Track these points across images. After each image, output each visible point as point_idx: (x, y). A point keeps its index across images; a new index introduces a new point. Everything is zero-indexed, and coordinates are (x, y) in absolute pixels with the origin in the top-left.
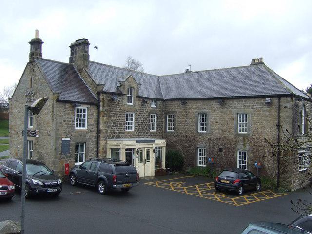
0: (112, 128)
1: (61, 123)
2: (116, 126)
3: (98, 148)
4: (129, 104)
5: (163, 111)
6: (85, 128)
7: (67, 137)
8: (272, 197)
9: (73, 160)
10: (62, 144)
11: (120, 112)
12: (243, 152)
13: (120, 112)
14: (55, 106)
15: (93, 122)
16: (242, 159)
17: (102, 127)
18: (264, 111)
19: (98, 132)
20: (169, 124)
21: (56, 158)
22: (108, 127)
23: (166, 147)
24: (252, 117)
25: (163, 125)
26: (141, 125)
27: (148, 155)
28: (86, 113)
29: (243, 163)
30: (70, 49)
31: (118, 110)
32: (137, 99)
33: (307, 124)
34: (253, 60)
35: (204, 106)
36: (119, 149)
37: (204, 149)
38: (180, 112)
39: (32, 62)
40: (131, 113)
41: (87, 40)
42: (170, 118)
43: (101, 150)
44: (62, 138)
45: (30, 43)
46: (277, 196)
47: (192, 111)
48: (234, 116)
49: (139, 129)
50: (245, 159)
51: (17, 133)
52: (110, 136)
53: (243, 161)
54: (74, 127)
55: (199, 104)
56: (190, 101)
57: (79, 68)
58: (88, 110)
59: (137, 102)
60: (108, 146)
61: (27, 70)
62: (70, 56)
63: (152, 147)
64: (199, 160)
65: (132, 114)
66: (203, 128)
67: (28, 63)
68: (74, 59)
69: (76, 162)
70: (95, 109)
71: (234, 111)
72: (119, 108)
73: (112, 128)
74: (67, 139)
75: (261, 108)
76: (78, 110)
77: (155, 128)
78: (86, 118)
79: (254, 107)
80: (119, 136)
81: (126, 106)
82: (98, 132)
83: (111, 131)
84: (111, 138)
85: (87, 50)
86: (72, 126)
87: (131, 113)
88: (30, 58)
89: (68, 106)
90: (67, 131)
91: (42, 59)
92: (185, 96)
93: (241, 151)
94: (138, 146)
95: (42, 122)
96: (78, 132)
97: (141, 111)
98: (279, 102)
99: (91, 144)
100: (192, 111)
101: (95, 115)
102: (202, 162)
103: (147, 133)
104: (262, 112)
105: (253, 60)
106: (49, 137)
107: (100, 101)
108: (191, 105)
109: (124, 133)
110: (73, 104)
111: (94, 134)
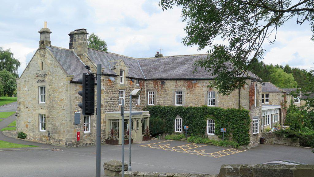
0: (109, 103)
1: (74, 100)
2: (112, 101)
4: (121, 83)
7: (78, 111)
8: (221, 152)
9: (82, 129)
10: (75, 117)
11: (114, 90)
13: (114, 90)
14: (68, 87)
16: (179, 124)
20: (150, 99)
22: (107, 102)
25: (145, 100)
27: (133, 125)
29: (211, 129)
30: (69, 37)
31: (114, 89)
32: (126, 79)
33: (258, 99)
39: (43, 49)
40: (122, 91)
41: (86, 30)
42: (151, 95)
44: (75, 111)
46: (240, 152)
49: (128, 103)
50: (180, 124)
52: (108, 109)
56: (168, 81)
57: (79, 53)
59: (127, 82)
62: (69, 43)
65: (123, 92)
66: (179, 102)
67: (38, 49)
68: (73, 46)
69: (84, 130)
73: (109, 103)
74: (78, 113)
80: (115, 109)
87: (122, 91)
88: (40, 45)
91: (50, 46)
92: (164, 76)
95: (56, 99)
102: (179, 129)
106: (64, 111)
109: (117, 107)
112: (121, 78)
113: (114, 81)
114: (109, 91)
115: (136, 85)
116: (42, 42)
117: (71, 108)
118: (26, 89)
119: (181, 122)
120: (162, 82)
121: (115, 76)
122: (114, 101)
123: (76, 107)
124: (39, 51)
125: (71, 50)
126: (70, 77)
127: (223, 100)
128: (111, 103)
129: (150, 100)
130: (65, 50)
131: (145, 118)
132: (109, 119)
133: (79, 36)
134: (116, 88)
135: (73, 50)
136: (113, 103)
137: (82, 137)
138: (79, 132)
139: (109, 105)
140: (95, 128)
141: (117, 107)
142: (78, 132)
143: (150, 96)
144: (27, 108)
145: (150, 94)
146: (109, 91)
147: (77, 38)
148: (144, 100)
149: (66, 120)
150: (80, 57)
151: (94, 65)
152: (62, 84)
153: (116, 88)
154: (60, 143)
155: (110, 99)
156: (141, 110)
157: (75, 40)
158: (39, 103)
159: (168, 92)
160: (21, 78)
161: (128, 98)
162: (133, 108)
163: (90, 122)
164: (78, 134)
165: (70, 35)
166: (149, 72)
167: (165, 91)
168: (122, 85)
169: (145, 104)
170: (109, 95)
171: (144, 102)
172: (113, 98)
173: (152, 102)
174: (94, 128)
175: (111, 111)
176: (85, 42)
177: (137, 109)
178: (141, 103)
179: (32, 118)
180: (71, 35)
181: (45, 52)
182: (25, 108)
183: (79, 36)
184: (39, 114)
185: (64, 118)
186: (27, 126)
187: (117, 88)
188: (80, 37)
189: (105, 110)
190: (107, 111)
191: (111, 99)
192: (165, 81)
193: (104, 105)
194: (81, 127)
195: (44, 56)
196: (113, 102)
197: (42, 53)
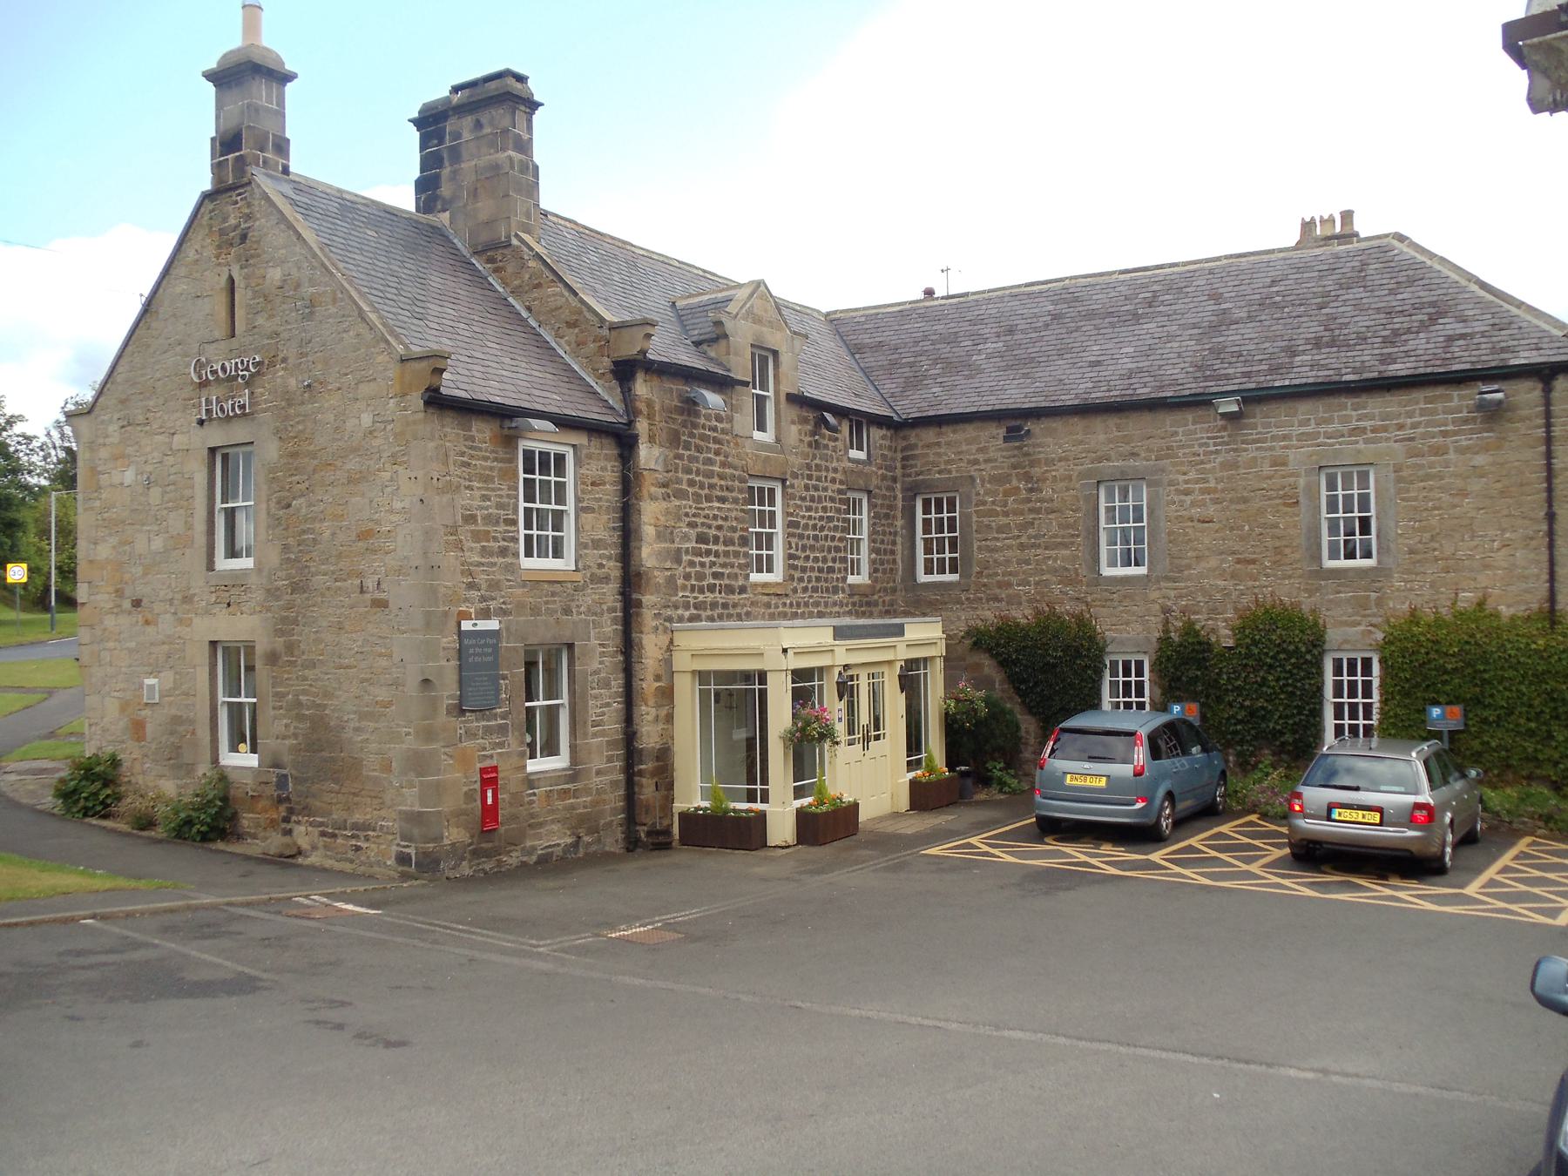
0: (692, 564)
2: (708, 552)
3: (628, 671)
4: (757, 435)
5: (894, 480)
6: (566, 564)
7: (485, 614)
11: (721, 477)
12: (1126, 665)
13: (721, 477)
15: (603, 527)
17: (648, 554)
18: (1462, 451)
19: (631, 581)
20: (928, 543)
21: (429, 734)
23: (946, 659)
24: (1399, 480)
25: (899, 547)
26: (812, 548)
28: (569, 479)
30: (414, 135)
32: (791, 413)
34: (1307, 226)
35: (1127, 440)
36: (762, 676)
37: (1359, 656)
38: (995, 480)
40: (767, 485)
41: (521, 79)
43: (648, 685)
44: (468, 617)
45: (210, 76)
47: (1060, 469)
48: (1302, 482)
51: (137, 603)
52: (687, 606)
53: (1353, 707)
54: (516, 555)
55: (1102, 432)
57: (484, 237)
58: (578, 463)
59: (794, 429)
60: (682, 662)
61: (198, 237)
62: (417, 174)
63: (890, 663)
64: (1329, 722)
65: (772, 491)
67: (206, 197)
68: (445, 190)
70: (607, 458)
71: (1297, 456)
72: (717, 453)
75: (1445, 434)
76: (529, 455)
77: (865, 567)
78: (570, 507)
79: (1408, 432)
80: (725, 606)
81: (748, 443)
82: (631, 581)
83: (687, 577)
84: (692, 619)
85: (526, 137)
86: (503, 552)
87: (767, 485)
88: (217, 168)
89: (483, 431)
90: (482, 579)
92: (1015, 395)
93: (1345, 657)
94: (843, 654)
96: (536, 583)
97: (810, 477)
98: (1548, 403)
99: (599, 658)
100: (1060, 469)
101: (609, 492)
103: (835, 590)
104: (1452, 456)
105: (1307, 226)
107: (631, 411)
108: (1052, 441)
109: (743, 590)
110: (504, 416)
111: (610, 593)
112: (761, 401)
113: (719, 419)
114: (691, 483)
115: (847, 453)
116: (227, 144)
117: (432, 592)
118: (129, 476)
119: (1146, 678)
120: (1009, 430)
121: (723, 383)
122: (721, 548)
123: (471, 586)
124: (209, 206)
125: (430, 218)
126: (424, 364)
127: (1434, 522)
128: (702, 565)
129: (928, 550)
130: (391, 213)
131: (912, 664)
132: (693, 672)
133: (484, 120)
134: (731, 466)
135: (445, 217)
136: (713, 564)
137: (516, 798)
138: (495, 769)
139: (687, 577)
140: (603, 734)
141: (743, 590)
142: (488, 763)
143: (927, 523)
144: (137, 603)
145: (926, 511)
146: (691, 483)
147: (467, 135)
148: (893, 552)
149: (396, 684)
150: (491, 260)
151: (582, 301)
152: (367, 419)
153: (731, 466)
154: (358, 848)
155: (693, 533)
156: (876, 610)
157: (455, 154)
158: (210, 566)
159: (1047, 492)
160: (97, 409)
161: (801, 537)
162: (835, 604)
163: (564, 700)
164: (489, 778)
165: (419, 123)
166: (914, 382)
167: (1031, 490)
168: (763, 446)
169: (898, 579)
170: (688, 505)
171: (894, 561)
172: (713, 532)
173: (941, 561)
174: (595, 735)
175: (704, 614)
176: (523, 157)
177: (854, 604)
178: (876, 571)
179: (168, 677)
180: (431, 122)
181: (249, 205)
182: (127, 604)
183: (478, 125)
184: (213, 644)
185: (383, 662)
186: (138, 728)
187: (736, 461)
188: (487, 130)
189: (669, 612)
190: (681, 619)
191: (702, 539)
192: (1028, 426)
193: (660, 577)
194: (502, 729)
195: (244, 237)
196: (717, 554)
197: (232, 221)
